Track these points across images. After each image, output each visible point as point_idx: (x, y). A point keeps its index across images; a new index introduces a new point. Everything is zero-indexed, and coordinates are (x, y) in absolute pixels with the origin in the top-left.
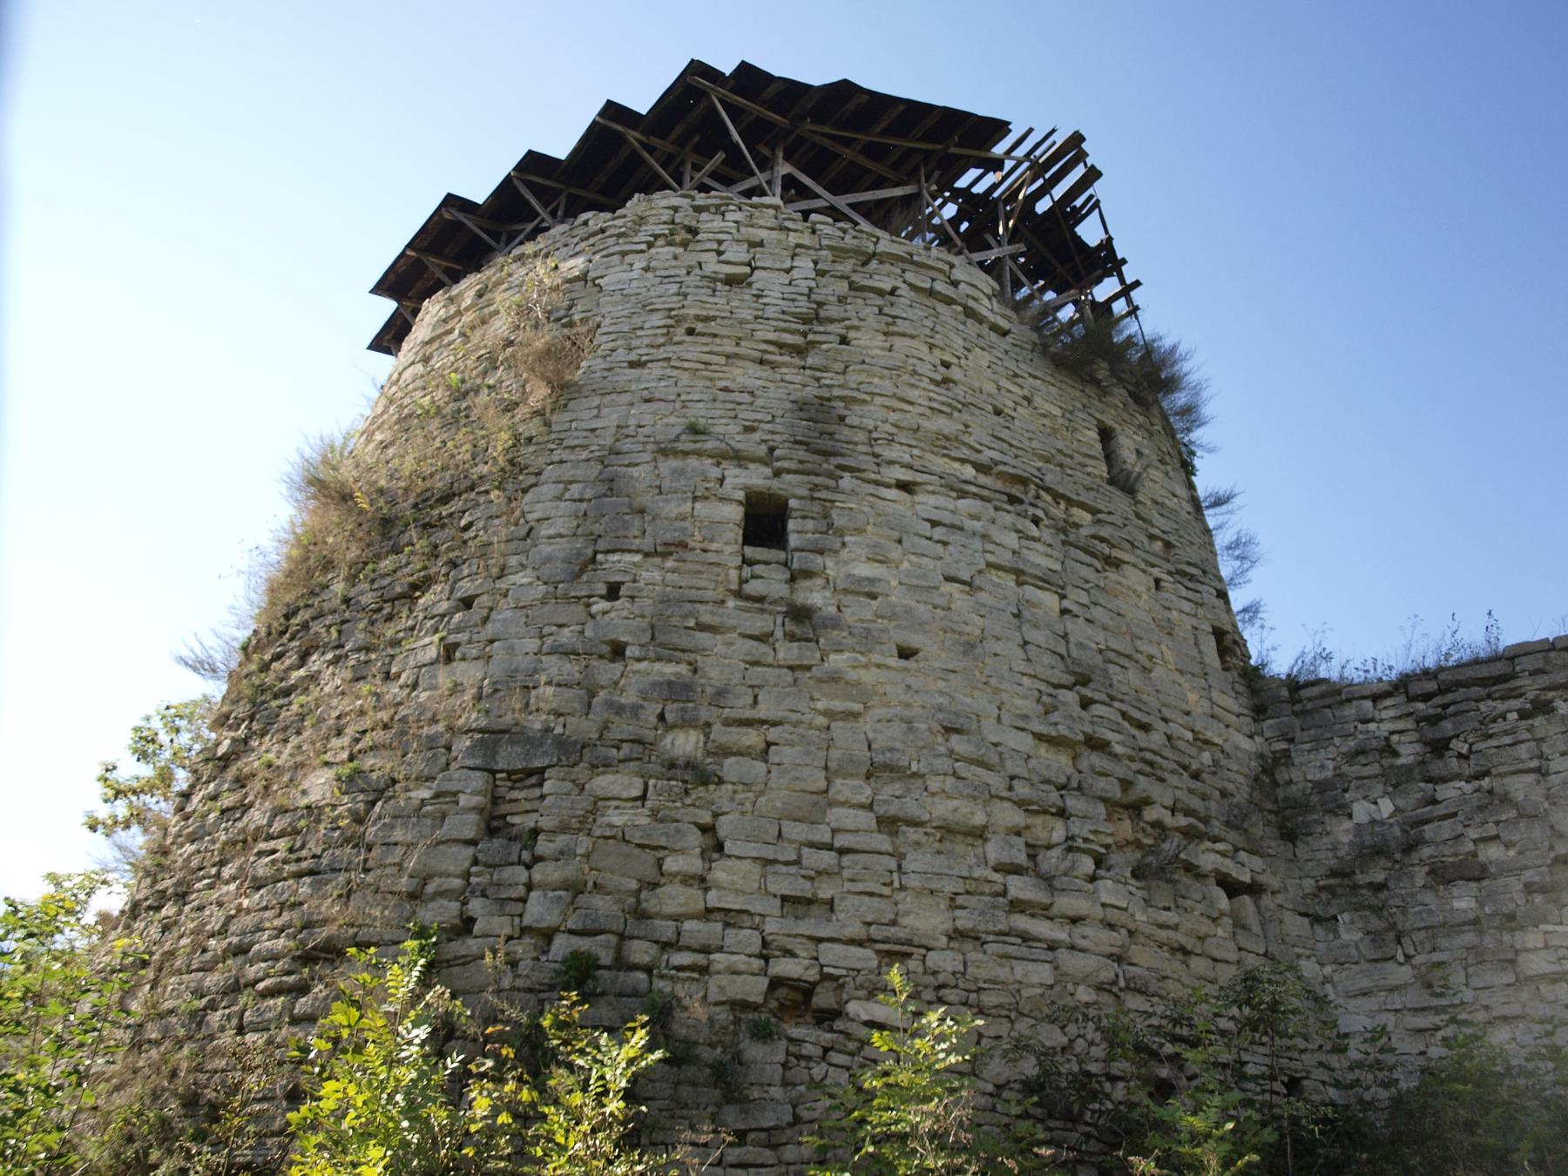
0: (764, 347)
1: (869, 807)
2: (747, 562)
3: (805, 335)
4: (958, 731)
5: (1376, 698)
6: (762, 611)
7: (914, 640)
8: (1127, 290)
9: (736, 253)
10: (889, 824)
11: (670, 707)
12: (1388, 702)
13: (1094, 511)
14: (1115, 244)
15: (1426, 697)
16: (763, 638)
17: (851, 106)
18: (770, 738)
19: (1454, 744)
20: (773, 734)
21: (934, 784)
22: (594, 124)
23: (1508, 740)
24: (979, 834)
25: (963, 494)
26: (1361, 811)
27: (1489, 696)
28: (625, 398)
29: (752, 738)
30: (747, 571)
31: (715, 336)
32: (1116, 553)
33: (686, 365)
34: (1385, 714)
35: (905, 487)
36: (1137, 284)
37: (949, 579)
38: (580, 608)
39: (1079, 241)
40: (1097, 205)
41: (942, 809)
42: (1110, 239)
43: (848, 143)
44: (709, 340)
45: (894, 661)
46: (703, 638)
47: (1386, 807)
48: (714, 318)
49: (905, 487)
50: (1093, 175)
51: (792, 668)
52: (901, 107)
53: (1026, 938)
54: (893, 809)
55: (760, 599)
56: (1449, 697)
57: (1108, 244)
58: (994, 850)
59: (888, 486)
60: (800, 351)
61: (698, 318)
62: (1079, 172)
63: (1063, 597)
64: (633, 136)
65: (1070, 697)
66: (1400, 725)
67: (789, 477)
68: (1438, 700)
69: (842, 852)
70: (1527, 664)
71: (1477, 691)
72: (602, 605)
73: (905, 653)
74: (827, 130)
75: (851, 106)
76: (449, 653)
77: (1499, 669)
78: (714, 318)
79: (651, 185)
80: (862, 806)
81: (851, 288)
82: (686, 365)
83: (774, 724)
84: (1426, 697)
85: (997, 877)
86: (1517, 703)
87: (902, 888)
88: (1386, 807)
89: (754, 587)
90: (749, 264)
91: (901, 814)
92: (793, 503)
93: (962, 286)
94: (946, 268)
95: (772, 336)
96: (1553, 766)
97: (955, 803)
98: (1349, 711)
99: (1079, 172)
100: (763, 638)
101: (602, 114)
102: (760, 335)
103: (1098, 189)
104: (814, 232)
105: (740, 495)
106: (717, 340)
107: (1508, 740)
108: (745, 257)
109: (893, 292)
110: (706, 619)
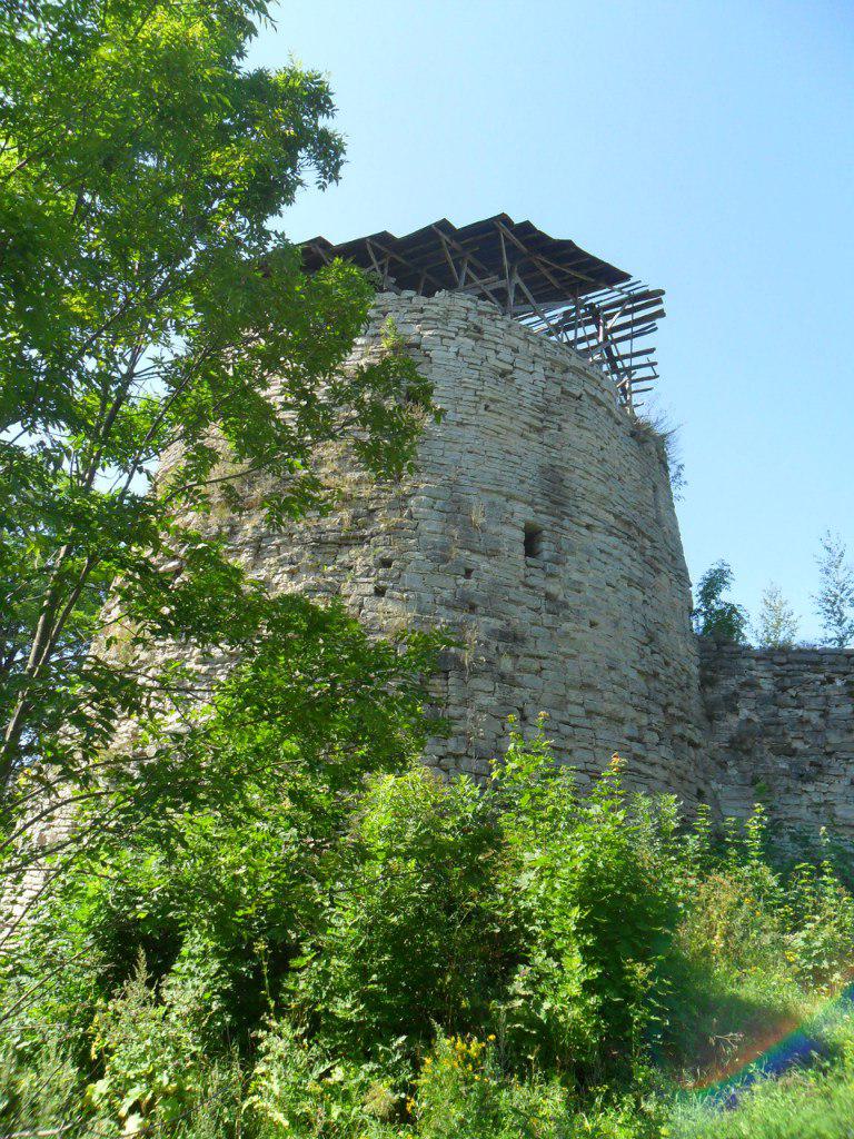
0: (524, 426)
1: (582, 705)
2: (529, 566)
3: (542, 421)
4: (614, 669)
5: (757, 659)
6: (534, 594)
7: (596, 619)
9: (506, 355)
10: (589, 714)
11: (501, 644)
12: (762, 662)
13: (652, 541)
15: (781, 664)
16: (536, 610)
17: (530, 236)
18: (544, 666)
20: (545, 663)
21: (606, 695)
22: (430, 227)
23: (814, 694)
24: (621, 721)
25: (611, 534)
26: (744, 713)
27: (808, 670)
28: (458, 447)
29: (536, 665)
30: (528, 572)
31: (500, 414)
32: (660, 566)
33: (488, 431)
34: (760, 668)
35: (588, 527)
37: (608, 585)
41: (609, 707)
43: (547, 266)
44: (498, 417)
45: (587, 628)
46: (512, 607)
48: (499, 401)
49: (588, 527)
51: (548, 628)
52: (573, 250)
53: (639, 772)
54: (592, 707)
55: (532, 587)
56: (790, 667)
58: (626, 730)
59: (582, 526)
60: (539, 431)
61: (492, 400)
63: (644, 594)
64: (445, 238)
65: (647, 650)
66: (766, 675)
67: (542, 516)
68: (786, 667)
69: (574, 726)
70: (831, 659)
73: (593, 625)
74: (543, 259)
75: (530, 236)
76: (379, 592)
77: (817, 658)
78: (499, 401)
79: (451, 285)
80: (577, 704)
81: (562, 392)
82: (488, 431)
83: (544, 658)
84: (781, 664)
85: (628, 743)
86: (822, 676)
87: (597, 746)
89: (532, 581)
90: (512, 364)
91: (593, 709)
92: (545, 533)
93: (606, 393)
94: (599, 379)
95: (528, 419)
97: (614, 706)
100: (536, 610)
101: (436, 224)
102: (521, 418)
104: (541, 345)
105: (522, 525)
106: (502, 418)
107: (814, 694)
108: (510, 359)
109: (579, 398)
110: (512, 596)
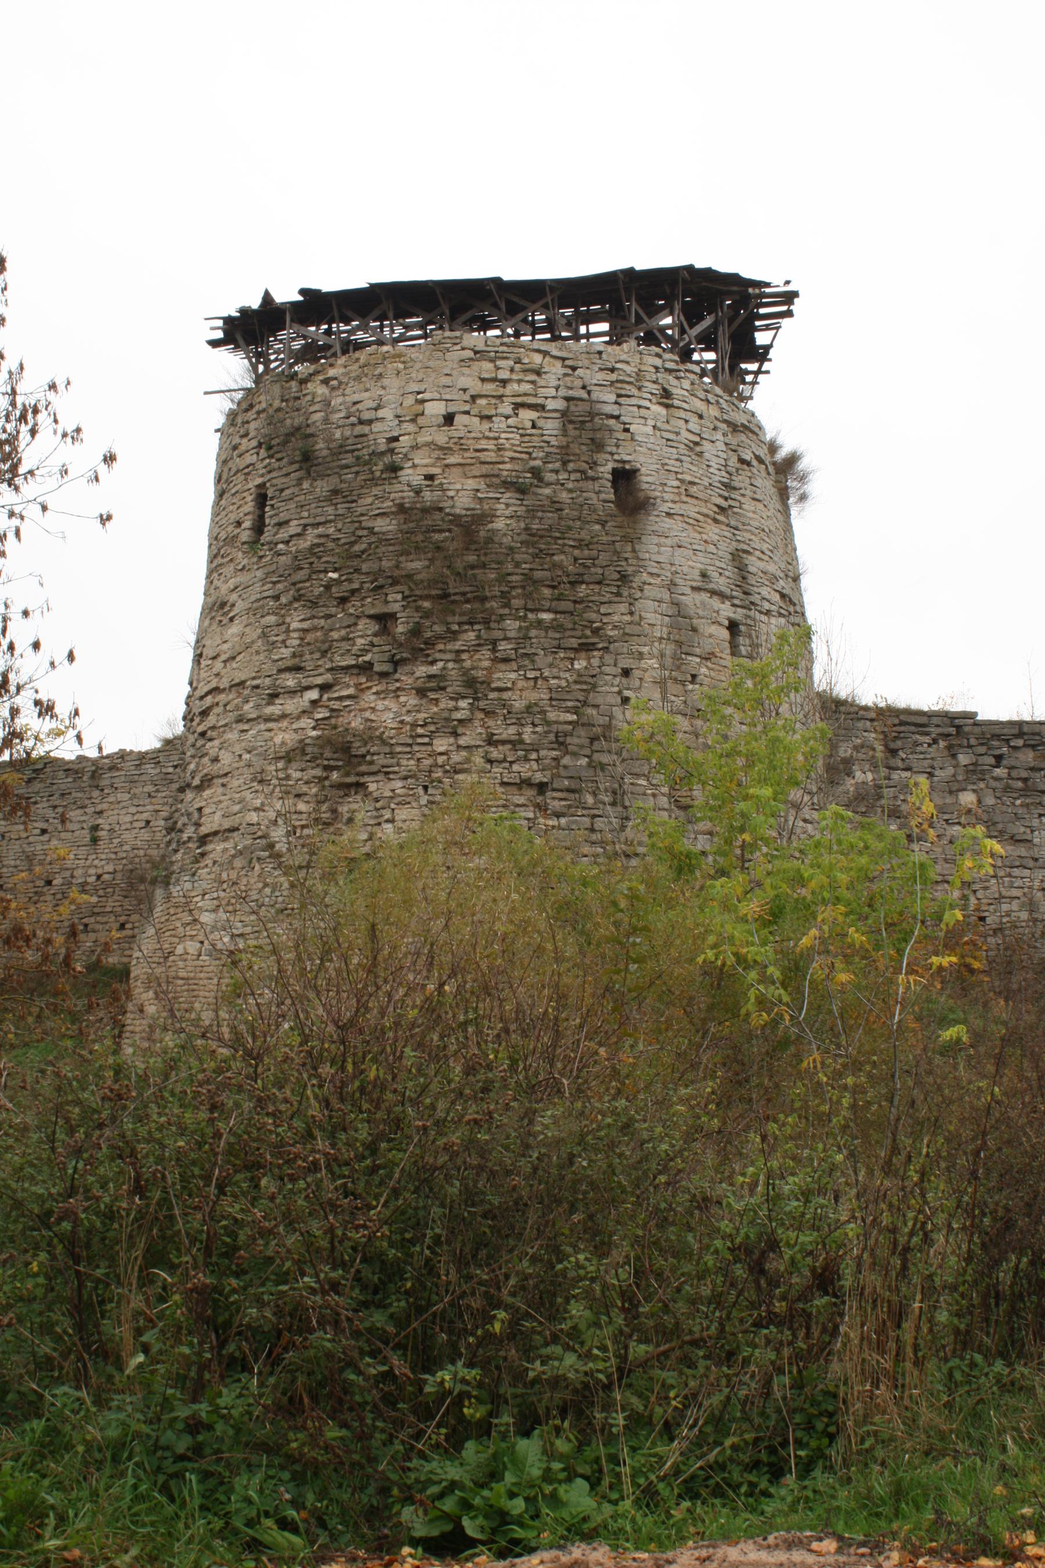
8: (758, 372)
14: (771, 351)
19: (901, 753)
36: (767, 372)
38: (680, 687)
39: (753, 340)
40: (778, 328)
42: (770, 346)
47: (870, 776)
50: (789, 314)
56: (902, 728)
57: (767, 348)
62: (784, 308)
70: (935, 721)
71: (913, 728)
72: (690, 687)
77: (923, 720)
88: (870, 776)
96: (936, 773)
98: (860, 724)
99: (784, 308)
103: (785, 322)
